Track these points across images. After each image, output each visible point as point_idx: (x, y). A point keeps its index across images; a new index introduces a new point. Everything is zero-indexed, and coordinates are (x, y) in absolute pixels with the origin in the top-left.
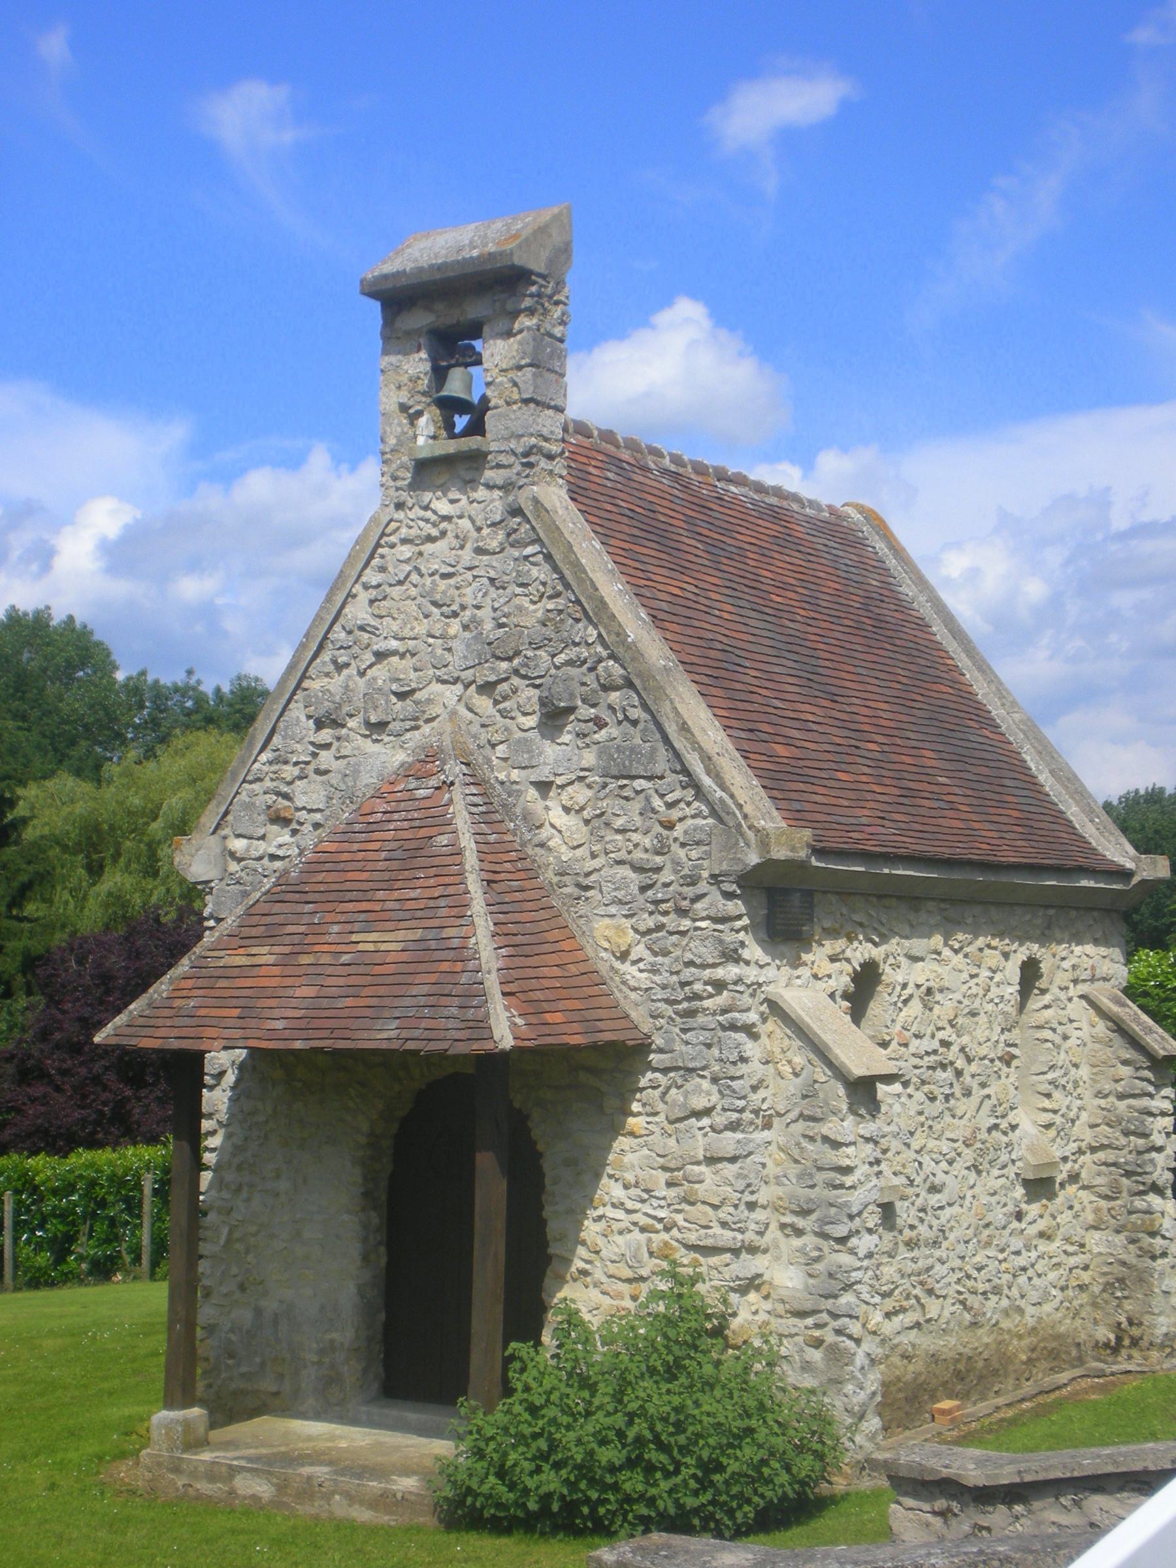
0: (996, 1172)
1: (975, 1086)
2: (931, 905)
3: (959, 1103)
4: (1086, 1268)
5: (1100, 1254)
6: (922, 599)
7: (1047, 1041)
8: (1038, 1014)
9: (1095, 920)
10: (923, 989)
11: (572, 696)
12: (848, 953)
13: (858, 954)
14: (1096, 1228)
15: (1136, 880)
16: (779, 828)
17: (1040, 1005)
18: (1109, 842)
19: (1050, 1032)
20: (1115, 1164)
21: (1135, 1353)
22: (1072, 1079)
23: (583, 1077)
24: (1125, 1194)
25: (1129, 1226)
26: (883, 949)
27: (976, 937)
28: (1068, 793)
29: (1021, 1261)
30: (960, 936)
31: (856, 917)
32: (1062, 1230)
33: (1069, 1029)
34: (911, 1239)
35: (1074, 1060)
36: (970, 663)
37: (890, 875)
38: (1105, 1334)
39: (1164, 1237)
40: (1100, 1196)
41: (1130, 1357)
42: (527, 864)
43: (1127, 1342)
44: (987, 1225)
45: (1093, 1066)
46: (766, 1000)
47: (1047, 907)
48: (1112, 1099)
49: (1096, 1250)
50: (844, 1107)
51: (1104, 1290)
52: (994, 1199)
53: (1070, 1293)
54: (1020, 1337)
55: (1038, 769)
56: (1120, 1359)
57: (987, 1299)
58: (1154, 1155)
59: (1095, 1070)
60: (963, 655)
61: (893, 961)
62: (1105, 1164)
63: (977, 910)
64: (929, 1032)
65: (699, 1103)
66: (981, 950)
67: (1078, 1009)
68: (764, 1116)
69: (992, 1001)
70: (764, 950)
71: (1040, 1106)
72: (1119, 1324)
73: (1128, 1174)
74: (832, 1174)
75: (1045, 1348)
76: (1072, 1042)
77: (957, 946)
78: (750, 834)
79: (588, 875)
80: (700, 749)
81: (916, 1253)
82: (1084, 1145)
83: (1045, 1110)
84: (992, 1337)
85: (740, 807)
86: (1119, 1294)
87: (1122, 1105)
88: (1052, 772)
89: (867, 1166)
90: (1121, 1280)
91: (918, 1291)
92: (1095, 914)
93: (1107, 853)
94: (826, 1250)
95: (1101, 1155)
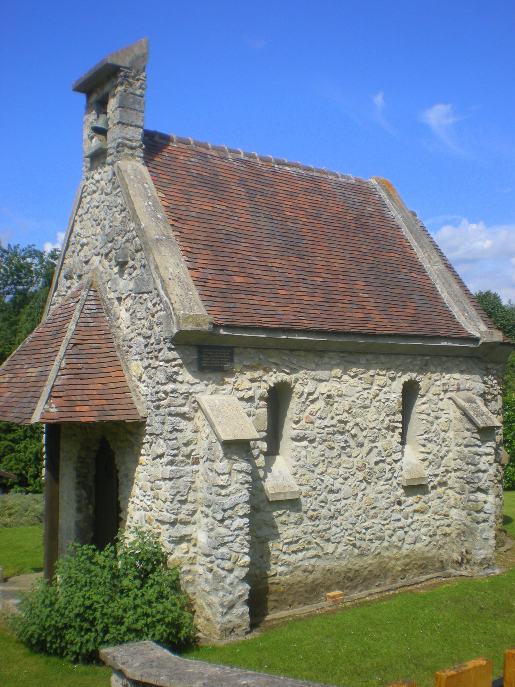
0: (382, 483)
1: (366, 441)
2: (331, 354)
3: (354, 451)
4: (449, 526)
5: (456, 519)
6: (399, 216)
7: (423, 420)
8: (420, 407)
9: (460, 362)
10: (325, 395)
11: (126, 256)
12: (265, 378)
13: (273, 378)
14: (455, 507)
15: (481, 342)
16: (186, 314)
17: (421, 402)
18: (471, 324)
19: (425, 415)
20: (462, 478)
21: (468, 566)
22: (441, 437)
23: (129, 436)
24: (467, 492)
25: (468, 507)
26: (293, 376)
27: (368, 370)
28: (454, 302)
29: (400, 524)
30: (354, 370)
31: (272, 360)
32: (432, 508)
33: (440, 414)
34: (312, 516)
35: (443, 429)
36: (416, 244)
37: (287, 339)
38: (456, 556)
39: (485, 513)
40: (457, 493)
41: (466, 568)
42: (109, 336)
43: (465, 561)
44: (374, 508)
45: (455, 431)
46: (195, 401)
47: (424, 355)
48: (462, 447)
49: (454, 517)
50: (221, 455)
51: (457, 537)
52: (380, 496)
53: (437, 538)
54: (397, 559)
55: (442, 291)
56: (462, 569)
57: (372, 543)
58: (480, 474)
59: (456, 433)
60: (414, 241)
61: (302, 382)
62: (458, 478)
63: (369, 357)
64: (329, 416)
65: (160, 451)
66: (372, 376)
67: (446, 404)
68: (193, 458)
69: (380, 400)
70: (194, 376)
71: (420, 450)
72: (462, 552)
73: (468, 483)
74: (217, 488)
75: (416, 564)
76: (443, 420)
77: (352, 374)
78: (174, 317)
79: (131, 340)
80: (160, 277)
81: (317, 522)
82: (450, 469)
83: (422, 452)
84: (375, 560)
85: (172, 304)
86: (463, 539)
87: (466, 450)
88: (448, 292)
89: (238, 485)
90: (463, 532)
91: (318, 540)
92: (461, 359)
93: (468, 330)
94: (215, 525)
95: (458, 474)
